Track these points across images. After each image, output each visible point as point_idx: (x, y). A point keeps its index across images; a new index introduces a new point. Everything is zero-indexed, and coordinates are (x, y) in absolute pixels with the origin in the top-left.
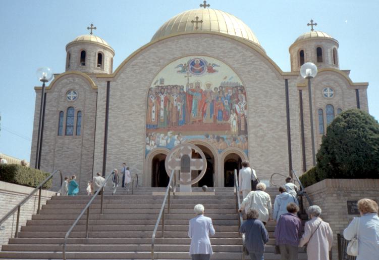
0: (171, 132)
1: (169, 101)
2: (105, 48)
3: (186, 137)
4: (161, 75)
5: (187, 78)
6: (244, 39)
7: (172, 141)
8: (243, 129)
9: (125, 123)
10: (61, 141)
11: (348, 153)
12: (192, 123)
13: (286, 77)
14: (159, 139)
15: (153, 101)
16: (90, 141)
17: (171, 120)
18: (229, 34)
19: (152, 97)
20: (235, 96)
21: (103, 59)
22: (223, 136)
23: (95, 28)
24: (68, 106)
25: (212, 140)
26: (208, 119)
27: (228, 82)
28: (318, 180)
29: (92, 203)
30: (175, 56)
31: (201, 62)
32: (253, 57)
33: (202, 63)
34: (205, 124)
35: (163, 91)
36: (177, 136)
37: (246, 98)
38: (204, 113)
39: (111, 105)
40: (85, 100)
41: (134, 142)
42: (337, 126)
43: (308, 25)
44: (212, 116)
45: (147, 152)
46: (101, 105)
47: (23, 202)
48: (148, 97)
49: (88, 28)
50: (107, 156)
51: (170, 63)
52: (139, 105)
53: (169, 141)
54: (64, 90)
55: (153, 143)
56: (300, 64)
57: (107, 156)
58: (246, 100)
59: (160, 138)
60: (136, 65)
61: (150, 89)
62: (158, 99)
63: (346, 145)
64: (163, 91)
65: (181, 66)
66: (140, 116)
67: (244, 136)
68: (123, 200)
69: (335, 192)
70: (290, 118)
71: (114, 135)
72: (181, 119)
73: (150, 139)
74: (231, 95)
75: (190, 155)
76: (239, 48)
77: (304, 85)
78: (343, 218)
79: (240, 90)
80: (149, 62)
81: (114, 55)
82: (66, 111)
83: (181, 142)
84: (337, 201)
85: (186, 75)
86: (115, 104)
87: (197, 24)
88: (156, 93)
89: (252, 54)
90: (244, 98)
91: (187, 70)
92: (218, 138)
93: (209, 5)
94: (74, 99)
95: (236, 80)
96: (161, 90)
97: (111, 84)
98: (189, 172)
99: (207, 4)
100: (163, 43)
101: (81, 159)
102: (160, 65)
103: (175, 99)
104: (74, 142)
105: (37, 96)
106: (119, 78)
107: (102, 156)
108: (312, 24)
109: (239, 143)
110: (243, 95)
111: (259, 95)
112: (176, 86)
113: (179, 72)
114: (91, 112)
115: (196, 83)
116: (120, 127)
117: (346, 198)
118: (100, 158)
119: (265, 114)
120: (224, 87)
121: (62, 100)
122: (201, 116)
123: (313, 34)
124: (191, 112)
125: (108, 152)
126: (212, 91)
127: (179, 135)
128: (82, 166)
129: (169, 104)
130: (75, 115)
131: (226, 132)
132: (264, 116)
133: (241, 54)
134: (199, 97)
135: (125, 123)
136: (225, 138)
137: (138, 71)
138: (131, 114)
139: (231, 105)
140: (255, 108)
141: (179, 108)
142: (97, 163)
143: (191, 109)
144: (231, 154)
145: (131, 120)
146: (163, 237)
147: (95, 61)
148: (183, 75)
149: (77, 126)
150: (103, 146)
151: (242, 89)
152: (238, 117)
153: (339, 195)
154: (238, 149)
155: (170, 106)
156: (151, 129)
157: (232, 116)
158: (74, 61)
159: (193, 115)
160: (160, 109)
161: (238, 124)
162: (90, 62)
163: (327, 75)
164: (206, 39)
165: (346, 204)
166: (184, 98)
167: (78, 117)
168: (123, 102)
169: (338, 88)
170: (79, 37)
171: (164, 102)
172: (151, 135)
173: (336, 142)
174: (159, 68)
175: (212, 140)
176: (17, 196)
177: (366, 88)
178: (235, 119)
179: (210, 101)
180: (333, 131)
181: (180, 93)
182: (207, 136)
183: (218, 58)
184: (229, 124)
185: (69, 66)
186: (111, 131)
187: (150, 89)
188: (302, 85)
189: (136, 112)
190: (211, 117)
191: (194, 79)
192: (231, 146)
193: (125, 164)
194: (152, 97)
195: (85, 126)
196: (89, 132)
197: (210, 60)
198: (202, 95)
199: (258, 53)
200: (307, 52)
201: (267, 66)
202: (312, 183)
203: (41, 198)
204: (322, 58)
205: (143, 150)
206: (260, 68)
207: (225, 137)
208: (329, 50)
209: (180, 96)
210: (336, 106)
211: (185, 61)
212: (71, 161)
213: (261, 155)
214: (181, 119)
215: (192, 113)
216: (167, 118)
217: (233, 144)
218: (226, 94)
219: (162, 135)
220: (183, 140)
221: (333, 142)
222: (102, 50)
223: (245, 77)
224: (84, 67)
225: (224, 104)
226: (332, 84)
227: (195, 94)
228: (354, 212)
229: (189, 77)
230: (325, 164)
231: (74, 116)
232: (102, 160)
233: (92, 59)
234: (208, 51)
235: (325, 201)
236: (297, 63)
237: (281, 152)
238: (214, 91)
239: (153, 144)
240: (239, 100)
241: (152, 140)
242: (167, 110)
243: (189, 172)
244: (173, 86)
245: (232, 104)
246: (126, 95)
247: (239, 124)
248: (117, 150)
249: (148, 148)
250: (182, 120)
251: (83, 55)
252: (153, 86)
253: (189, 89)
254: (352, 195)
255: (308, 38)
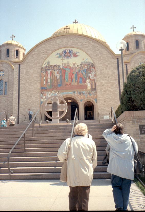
0: (54, 91)
1: (53, 74)
2: (20, 47)
3: (62, 93)
5: (62, 60)
6: (97, 39)
8: (94, 87)
11: (140, 93)
13: (118, 57)
17: (54, 84)
18: (83, 34)
19: (43, 72)
21: (19, 54)
23: (15, 37)
26: (74, 83)
27: (85, 62)
28: (122, 112)
29: (27, 131)
31: (70, 51)
32: (98, 47)
34: (73, 85)
35: (49, 68)
37: (95, 70)
38: (72, 80)
39: (21, 77)
40: (9, 76)
41: (34, 97)
42: (133, 75)
43: (131, 28)
46: (16, 78)
48: (41, 72)
49: (11, 37)
50: (20, 105)
51: (53, 52)
52: (36, 77)
55: (45, 97)
56: (126, 50)
58: (95, 72)
60: (34, 55)
61: (42, 68)
62: (47, 73)
63: (138, 88)
64: (49, 68)
65: (58, 54)
66: (37, 83)
67: (94, 91)
68: (8, 130)
69: (131, 120)
71: (23, 94)
72: (59, 83)
73: (43, 95)
76: (91, 42)
77: (128, 62)
78: (137, 137)
79: (92, 66)
80: (41, 52)
81: (25, 51)
84: (133, 126)
86: (23, 77)
87: (67, 30)
88: (46, 70)
89: (98, 45)
91: (62, 56)
92: (80, 93)
93: (78, 22)
94: (3, 75)
95: (90, 60)
96: (48, 68)
97: (21, 66)
98: (57, 112)
100: (49, 41)
101: (8, 108)
102: (47, 54)
103: (56, 72)
106: (25, 62)
107: (17, 105)
108: (133, 28)
109: (92, 96)
110: (93, 69)
111: (102, 68)
112: (56, 65)
115: (67, 63)
117: (139, 123)
119: (106, 79)
120: (83, 65)
122: (70, 81)
123: (134, 33)
127: (58, 92)
128: (8, 111)
129: (52, 76)
130: (4, 84)
131: (84, 89)
132: (106, 80)
134: (69, 71)
137: (35, 58)
140: (100, 75)
141: (58, 77)
142: (15, 110)
143: (65, 77)
144: (88, 102)
146: (24, 152)
147: (14, 54)
148: (60, 59)
150: (18, 100)
151: (93, 65)
152: (91, 81)
153: (134, 122)
154: (92, 99)
156: (43, 89)
157: (87, 80)
159: (66, 81)
161: (91, 84)
163: (141, 56)
164: (72, 38)
165: (138, 128)
168: (28, 76)
170: (6, 42)
173: (132, 86)
174: (46, 56)
179: (75, 72)
180: (130, 79)
181: (59, 69)
182: (74, 92)
183: (79, 48)
184: (86, 85)
187: (42, 68)
188: (128, 62)
189: (35, 81)
190: (76, 81)
191: (66, 61)
192: (88, 97)
193: (29, 109)
194: (43, 72)
195: (9, 90)
197: (74, 50)
199: (103, 45)
201: (106, 52)
202: (120, 115)
204: (139, 47)
205: (39, 102)
206: (103, 53)
207: (84, 92)
208: (143, 42)
211: (61, 51)
212: (2, 109)
213: (104, 102)
214: (59, 83)
215: (65, 80)
216: (52, 83)
217: (88, 96)
219: (49, 93)
220: (61, 95)
221: (130, 86)
222: (18, 48)
223: (95, 58)
224: (9, 58)
225: (83, 74)
228: (144, 133)
229: (63, 60)
230: (125, 101)
231: (3, 85)
232: (17, 108)
233: (13, 53)
235: (125, 126)
238: (77, 67)
239: (45, 98)
241: (44, 96)
242: (51, 79)
243: (57, 112)
244: (55, 66)
245: (87, 74)
246: (29, 71)
247: (91, 85)
249: (42, 100)
251: (8, 51)
252: (44, 66)
254: (143, 121)
255: (131, 35)
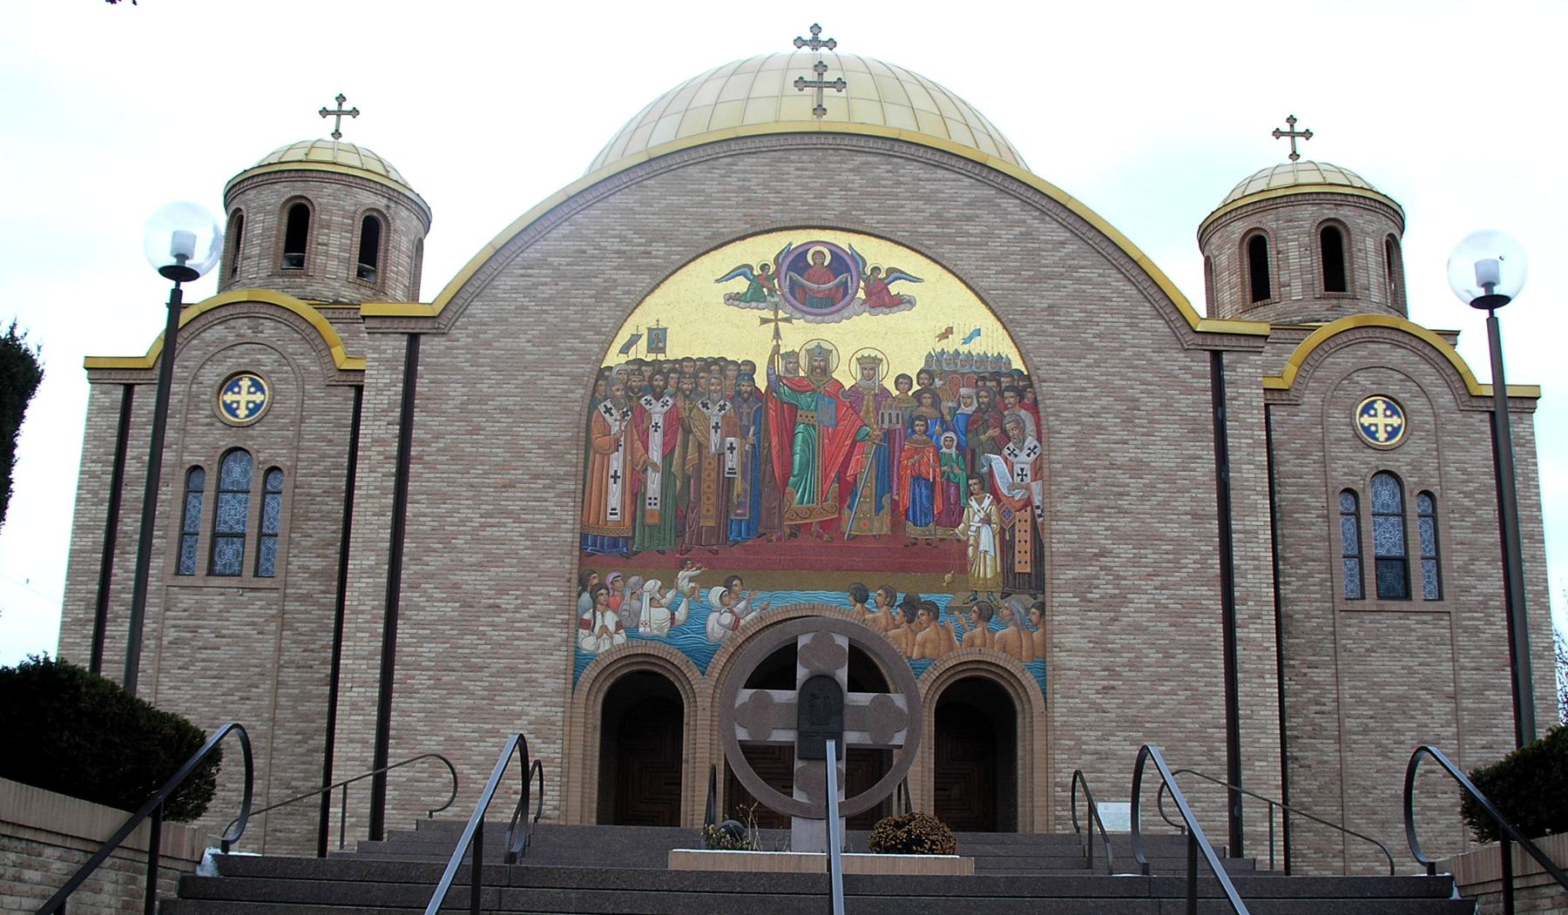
0: (693, 573)
1: (688, 432)
4: (641, 321)
7: (699, 613)
8: (1023, 566)
9: (483, 526)
10: (187, 600)
12: (793, 535)
14: (635, 603)
15: (615, 429)
16: (316, 603)
17: (691, 516)
20: (990, 414)
22: (933, 598)
23: (354, 112)
24: (226, 443)
25: (880, 613)
30: (720, 227)
32: (1069, 248)
33: (842, 263)
34: (853, 538)
36: (718, 590)
38: (847, 490)
44: (886, 500)
45: (579, 661)
47: (75, 882)
50: (398, 674)
52: (546, 445)
53: (681, 614)
54: (212, 375)
55: (610, 619)
57: (397, 675)
59: (640, 600)
61: (602, 374)
62: (639, 419)
64: (659, 381)
67: (1028, 600)
70: (1235, 525)
74: (969, 410)
75: (842, 675)
82: (215, 467)
83: (737, 620)
85: (769, 314)
86: (437, 437)
90: (1030, 427)
94: (252, 412)
95: (994, 342)
96: (651, 378)
97: (425, 345)
99: (823, 37)
104: (244, 605)
105: (92, 396)
110: (1023, 413)
113: (733, 299)
114: (326, 473)
116: (458, 542)
118: (364, 684)
121: (202, 416)
124: (785, 484)
125: (403, 655)
126: (885, 391)
127: (728, 585)
128: (280, 715)
130: (256, 485)
131: (948, 577)
132: (1122, 511)
133: (1017, 230)
135: (483, 526)
136: (941, 606)
137: (547, 292)
138: (511, 485)
139: (970, 456)
141: (732, 461)
142: (354, 706)
145: (508, 513)
148: (752, 315)
149: (261, 535)
150: (380, 628)
152: (1005, 513)
155: (692, 454)
158: (256, 251)
160: (647, 464)
162: (326, 254)
166: (759, 417)
167: (265, 493)
168: (477, 430)
169: (1418, 404)
171: (665, 435)
172: (601, 586)
174: (646, 279)
175: (880, 614)
176: (48, 851)
177: (1532, 410)
178: (987, 520)
181: (739, 393)
182: (861, 596)
185: (235, 270)
186: (417, 560)
189: (536, 477)
190: (879, 508)
191: (799, 335)
194: (608, 410)
196: (316, 564)
197: (877, 254)
198: (838, 409)
200: (1281, 246)
203: (161, 862)
206: (1104, 298)
207: (942, 600)
209: (736, 408)
210: (1410, 481)
211: (763, 250)
212: (229, 693)
214: (741, 513)
217: (978, 630)
218: (947, 404)
219: (652, 585)
220: (747, 611)
225: (938, 449)
226: (1393, 389)
227: (805, 400)
232: (375, 693)
234: (870, 211)
236: (1238, 297)
237: (1195, 673)
238: (895, 393)
239: (612, 627)
240: (1006, 437)
245: (973, 452)
247: (1006, 547)
248: (440, 648)
249: (588, 643)
250: (712, 523)
251: (298, 220)
253: (779, 378)
